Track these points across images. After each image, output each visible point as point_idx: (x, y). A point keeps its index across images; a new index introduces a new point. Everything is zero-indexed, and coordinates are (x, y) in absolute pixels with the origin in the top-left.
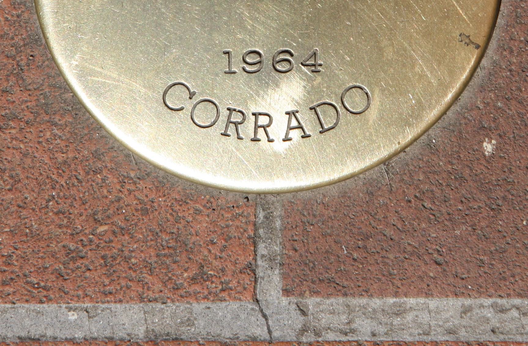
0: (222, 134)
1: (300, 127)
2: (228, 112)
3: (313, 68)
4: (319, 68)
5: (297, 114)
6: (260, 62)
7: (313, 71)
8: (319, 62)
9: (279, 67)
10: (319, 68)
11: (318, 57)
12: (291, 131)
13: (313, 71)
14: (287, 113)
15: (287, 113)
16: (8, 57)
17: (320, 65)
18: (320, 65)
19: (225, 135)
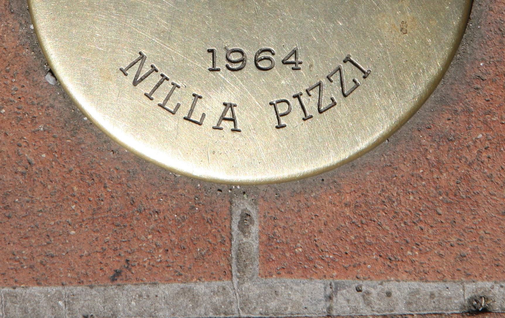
0: (146, 95)
1: (233, 120)
2: (224, 107)
3: (294, 66)
4: (299, 66)
5: (235, 108)
6: (242, 60)
7: (293, 69)
8: (299, 60)
9: (260, 65)
10: (299, 66)
11: (299, 54)
12: (223, 122)
13: (293, 69)
14: (225, 104)
15: (225, 104)
16: (94, 232)
17: (300, 63)
18: (300, 63)
19: (148, 96)
